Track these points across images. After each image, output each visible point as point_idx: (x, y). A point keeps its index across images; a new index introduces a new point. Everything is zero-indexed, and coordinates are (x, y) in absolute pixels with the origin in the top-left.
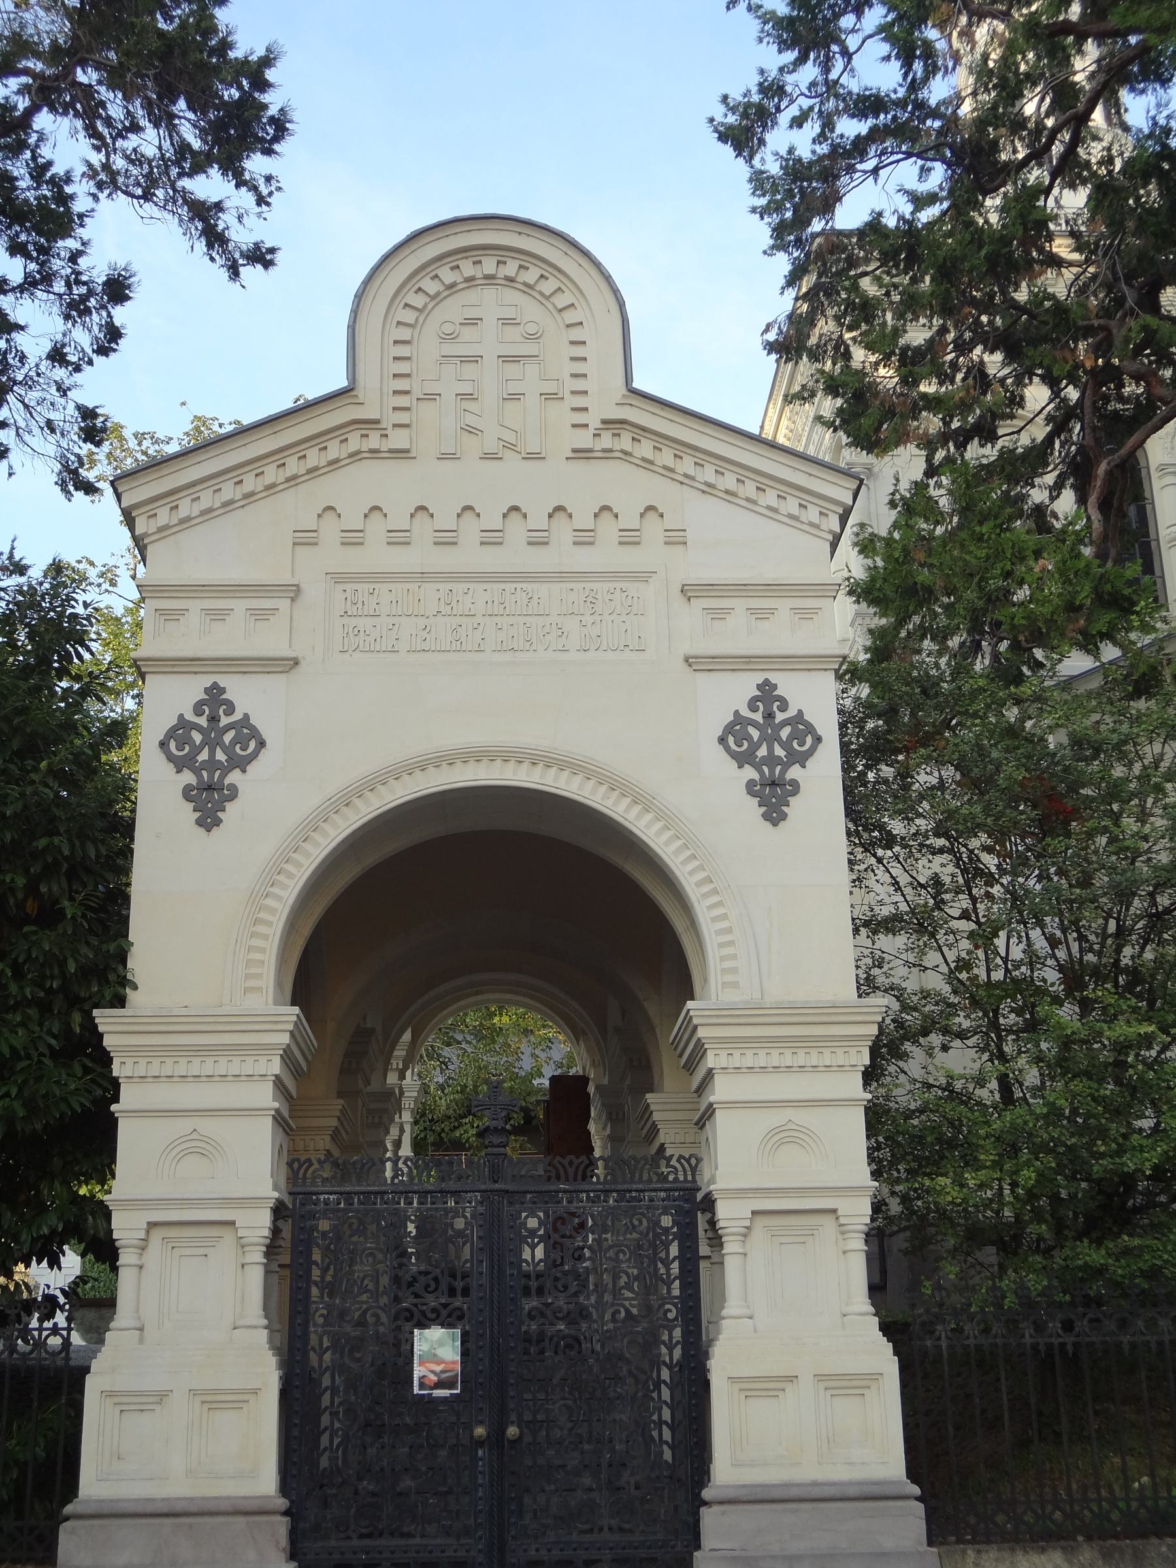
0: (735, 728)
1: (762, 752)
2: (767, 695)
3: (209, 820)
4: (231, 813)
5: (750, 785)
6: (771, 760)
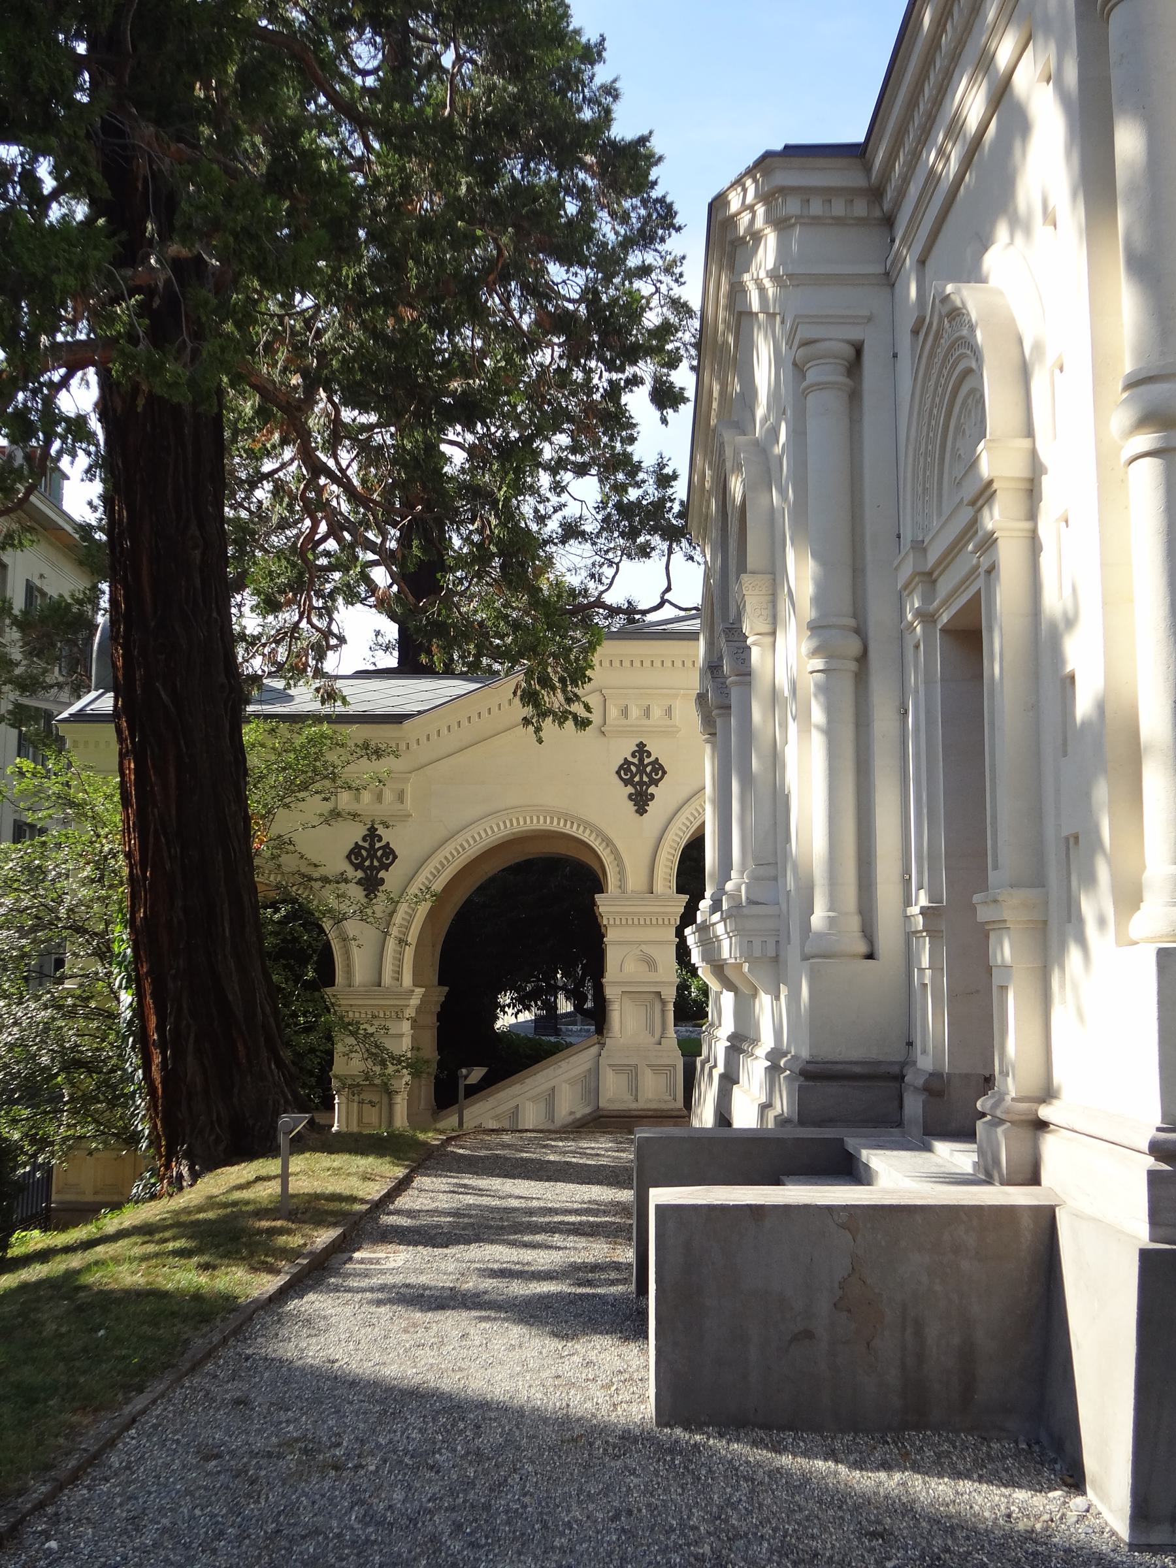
0: (625, 767)
1: (637, 779)
2: (641, 749)
3: (641, 811)
4: (652, 807)
5: (630, 797)
6: (641, 783)
